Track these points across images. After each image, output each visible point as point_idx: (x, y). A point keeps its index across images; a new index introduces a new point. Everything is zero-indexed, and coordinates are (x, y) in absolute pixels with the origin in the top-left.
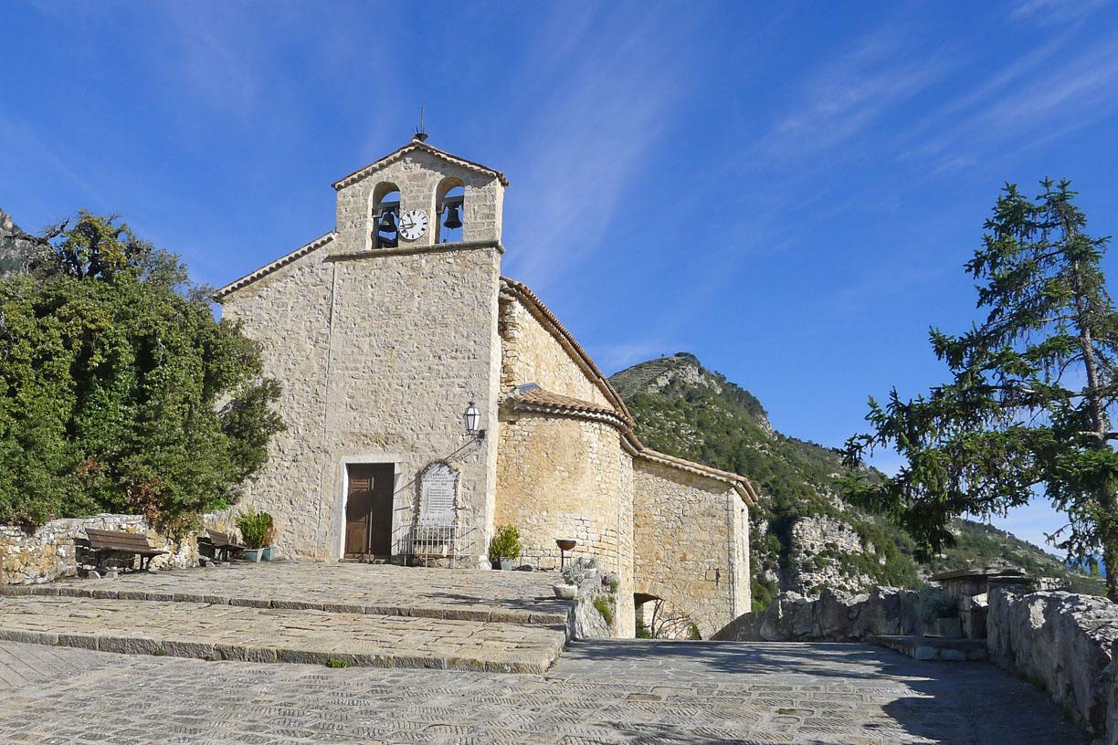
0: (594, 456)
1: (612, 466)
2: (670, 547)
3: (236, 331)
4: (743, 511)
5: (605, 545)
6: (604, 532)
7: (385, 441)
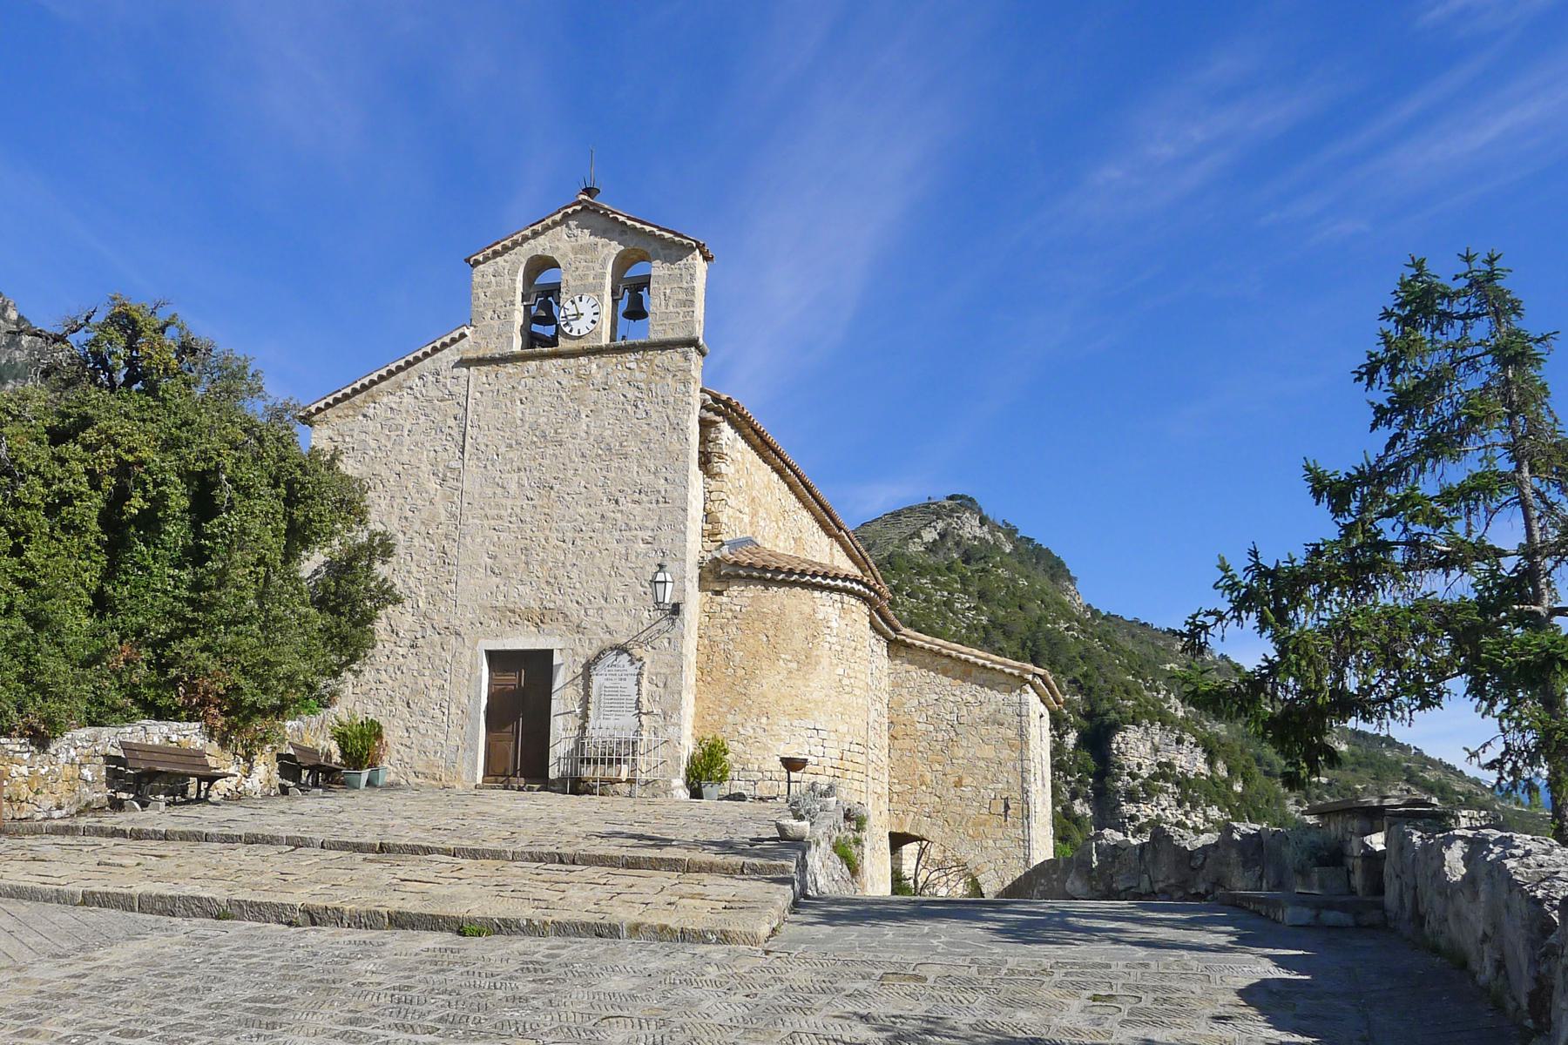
0: (834, 640)
4: (1041, 716)
5: (848, 765)
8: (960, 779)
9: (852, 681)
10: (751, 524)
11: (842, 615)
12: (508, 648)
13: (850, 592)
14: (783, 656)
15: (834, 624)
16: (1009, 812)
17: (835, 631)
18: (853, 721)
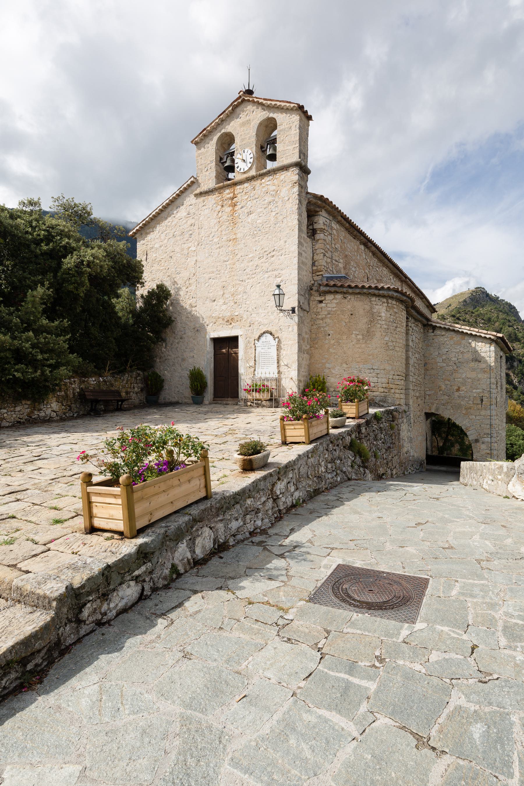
0: (384, 322)
1: (398, 329)
2: (449, 383)
3: (138, 282)
4: (501, 357)
5: (391, 386)
6: (391, 377)
7: (230, 321)
8: (459, 388)
9: (394, 343)
10: (345, 268)
11: (388, 309)
12: (221, 336)
13: (392, 298)
14: (354, 332)
15: (383, 314)
16: (483, 403)
17: (384, 318)
18: (395, 364)
